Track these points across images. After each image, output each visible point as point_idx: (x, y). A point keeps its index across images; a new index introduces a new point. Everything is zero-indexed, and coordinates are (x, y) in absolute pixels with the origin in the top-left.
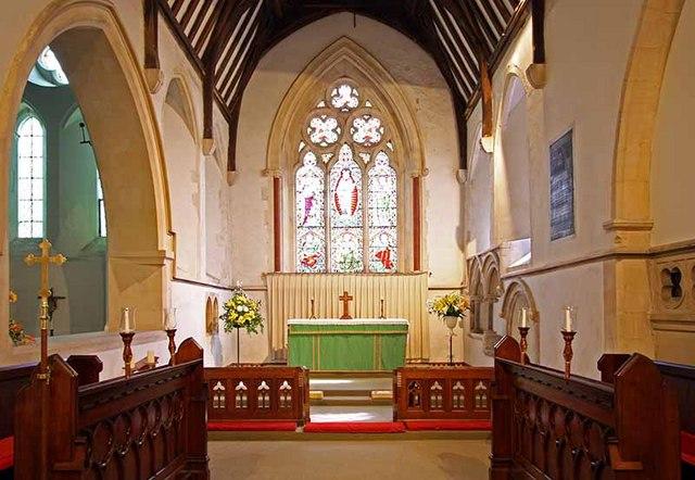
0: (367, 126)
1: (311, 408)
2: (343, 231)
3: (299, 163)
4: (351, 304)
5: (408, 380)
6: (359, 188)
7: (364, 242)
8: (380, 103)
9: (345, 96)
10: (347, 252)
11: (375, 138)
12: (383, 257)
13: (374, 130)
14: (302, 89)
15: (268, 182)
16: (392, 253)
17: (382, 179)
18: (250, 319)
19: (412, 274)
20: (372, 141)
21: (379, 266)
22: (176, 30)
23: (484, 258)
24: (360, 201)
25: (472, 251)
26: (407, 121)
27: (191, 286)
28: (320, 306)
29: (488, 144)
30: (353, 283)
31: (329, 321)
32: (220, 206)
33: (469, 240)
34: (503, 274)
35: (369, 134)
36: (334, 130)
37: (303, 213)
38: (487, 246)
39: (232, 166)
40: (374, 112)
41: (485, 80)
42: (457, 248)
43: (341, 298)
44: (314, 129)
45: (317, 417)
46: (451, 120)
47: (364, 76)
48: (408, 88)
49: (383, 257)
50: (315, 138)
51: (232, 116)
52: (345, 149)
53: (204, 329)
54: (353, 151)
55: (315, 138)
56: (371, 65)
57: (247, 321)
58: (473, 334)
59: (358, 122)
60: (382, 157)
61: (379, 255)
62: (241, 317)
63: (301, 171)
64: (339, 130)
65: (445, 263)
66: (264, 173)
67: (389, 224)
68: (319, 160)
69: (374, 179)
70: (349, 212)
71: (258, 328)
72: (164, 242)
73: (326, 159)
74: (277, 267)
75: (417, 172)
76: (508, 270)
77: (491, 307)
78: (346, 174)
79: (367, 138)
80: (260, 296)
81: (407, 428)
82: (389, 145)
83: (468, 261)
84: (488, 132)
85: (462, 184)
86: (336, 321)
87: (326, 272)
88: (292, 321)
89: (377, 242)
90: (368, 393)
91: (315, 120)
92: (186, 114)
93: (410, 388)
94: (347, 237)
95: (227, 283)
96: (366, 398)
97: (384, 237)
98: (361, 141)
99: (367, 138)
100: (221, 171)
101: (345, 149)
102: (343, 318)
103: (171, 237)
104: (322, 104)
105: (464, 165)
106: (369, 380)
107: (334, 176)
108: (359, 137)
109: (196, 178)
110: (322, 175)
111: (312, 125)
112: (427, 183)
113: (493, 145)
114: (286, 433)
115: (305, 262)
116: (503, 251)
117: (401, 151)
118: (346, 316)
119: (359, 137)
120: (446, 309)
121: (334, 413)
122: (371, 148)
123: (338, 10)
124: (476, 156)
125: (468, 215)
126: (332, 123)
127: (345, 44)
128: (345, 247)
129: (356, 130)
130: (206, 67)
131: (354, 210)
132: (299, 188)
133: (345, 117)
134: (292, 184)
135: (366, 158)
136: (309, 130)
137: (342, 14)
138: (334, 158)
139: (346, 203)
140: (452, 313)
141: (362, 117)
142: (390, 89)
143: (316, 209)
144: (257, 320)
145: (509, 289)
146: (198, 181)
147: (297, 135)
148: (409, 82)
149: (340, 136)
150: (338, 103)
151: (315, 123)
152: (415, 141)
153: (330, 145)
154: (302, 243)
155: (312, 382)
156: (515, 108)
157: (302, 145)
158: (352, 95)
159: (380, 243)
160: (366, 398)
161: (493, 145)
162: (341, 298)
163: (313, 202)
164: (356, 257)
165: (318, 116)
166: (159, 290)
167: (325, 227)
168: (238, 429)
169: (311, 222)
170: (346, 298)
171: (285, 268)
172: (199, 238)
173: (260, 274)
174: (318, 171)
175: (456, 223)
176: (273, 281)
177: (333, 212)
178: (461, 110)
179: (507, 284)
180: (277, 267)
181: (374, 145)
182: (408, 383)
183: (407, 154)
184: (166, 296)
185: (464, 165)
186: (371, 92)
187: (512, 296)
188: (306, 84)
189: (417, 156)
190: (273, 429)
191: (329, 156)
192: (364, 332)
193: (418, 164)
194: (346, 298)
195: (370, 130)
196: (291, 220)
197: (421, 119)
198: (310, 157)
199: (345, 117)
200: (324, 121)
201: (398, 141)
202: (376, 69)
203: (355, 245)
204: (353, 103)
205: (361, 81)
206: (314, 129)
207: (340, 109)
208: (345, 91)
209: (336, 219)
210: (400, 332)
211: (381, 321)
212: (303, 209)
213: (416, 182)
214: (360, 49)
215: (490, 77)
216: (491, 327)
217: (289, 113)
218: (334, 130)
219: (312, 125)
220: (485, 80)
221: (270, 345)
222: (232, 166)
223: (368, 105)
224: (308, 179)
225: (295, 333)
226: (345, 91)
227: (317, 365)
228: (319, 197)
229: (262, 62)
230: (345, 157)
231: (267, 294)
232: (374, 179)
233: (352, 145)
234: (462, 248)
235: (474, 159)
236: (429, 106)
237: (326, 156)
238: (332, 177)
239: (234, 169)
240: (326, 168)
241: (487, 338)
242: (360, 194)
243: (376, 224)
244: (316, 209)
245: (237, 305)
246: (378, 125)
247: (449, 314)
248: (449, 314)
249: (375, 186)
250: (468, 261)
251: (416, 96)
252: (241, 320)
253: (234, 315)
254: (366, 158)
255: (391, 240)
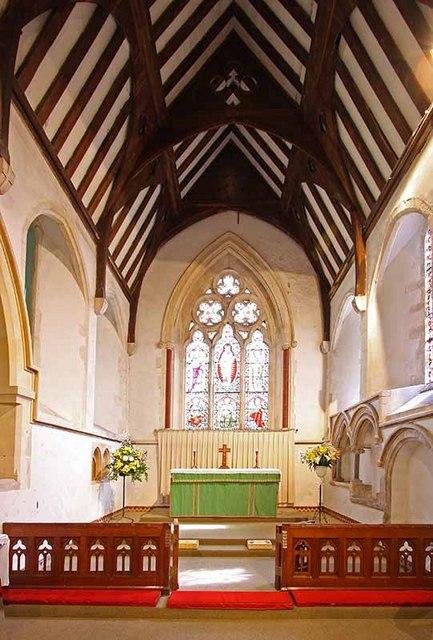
0: (246, 309)
1: (181, 561)
2: (224, 395)
3: (188, 338)
4: (229, 455)
5: (295, 540)
6: (238, 360)
7: (239, 404)
8: (257, 290)
9: (229, 285)
10: (226, 413)
11: (252, 319)
12: (257, 417)
13: (251, 312)
14: (193, 277)
15: (161, 354)
16: (264, 415)
17: (257, 353)
18: (134, 468)
19: (281, 431)
20: (250, 321)
21: (253, 425)
22: (117, 272)
23: (352, 413)
24: (238, 371)
25: (333, 409)
26: (279, 302)
27: (72, 434)
28: (201, 458)
29: (361, 301)
30: (231, 438)
31: (244, 471)
32: (119, 371)
33: (331, 401)
34: (383, 422)
35: (247, 316)
36: (219, 313)
37: (190, 381)
38: (354, 399)
39: (131, 338)
40: (253, 297)
41: (360, 243)
42: (319, 407)
43: (221, 450)
44: (202, 312)
45: (192, 578)
46: (316, 301)
47: (248, 269)
48: (282, 274)
49: (257, 417)
50: (203, 319)
51: (133, 296)
52: (228, 328)
53: (90, 477)
54: (234, 330)
55: (203, 319)
56: (251, 255)
57: (132, 470)
58: (337, 483)
59: (238, 306)
60: (257, 335)
61: (253, 415)
62: (126, 466)
63: (191, 346)
64: (223, 313)
65: (310, 421)
66: (159, 345)
67: (261, 390)
68: (206, 337)
69: (251, 353)
70: (230, 380)
71: (143, 476)
72: (20, 379)
73: (211, 336)
74: (167, 425)
75: (287, 344)
76: (388, 418)
77: (358, 457)
78: (228, 348)
79: (246, 319)
80: (151, 449)
81: (296, 604)
82: (263, 324)
83: (331, 418)
84: (360, 290)
85: (325, 354)
86: (216, 471)
87: (209, 429)
88: (173, 471)
89: (251, 405)
90: (244, 543)
91: (203, 304)
92: (75, 268)
93: (298, 549)
94: (227, 401)
95: (124, 436)
96: (241, 548)
97: (258, 401)
98: (240, 321)
99: (246, 319)
100: (118, 339)
101: (228, 328)
102: (222, 467)
103: (31, 376)
104: (209, 291)
105: (327, 336)
106: (244, 525)
107: (218, 350)
108: (239, 319)
109: (84, 331)
110: (208, 348)
111: (201, 309)
112: (295, 354)
113: (368, 303)
114: (145, 609)
115: (192, 421)
116: (384, 400)
117: (274, 329)
118: (224, 466)
119: (239, 319)
120: (318, 460)
121: (208, 567)
122: (249, 327)
123: (225, 209)
124: (339, 329)
125: (331, 380)
126: (217, 307)
127: (229, 239)
128: (225, 408)
129: (237, 312)
130: (102, 232)
131: (233, 378)
132: (188, 360)
133: (227, 302)
134: (183, 355)
135: (245, 335)
136: (198, 312)
137: (228, 212)
138: (218, 333)
139: (227, 372)
140: (324, 463)
141: (242, 301)
142: (267, 276)
143: (202, 378)
144: (142, 469)
145: (393, 437)
146: (86, 335)
147: (189, 318)
148: (282, 269)
149: (223, 318)
150: (222, 291)
151: (204, 307)
152: (286, 319)
153: (215, 324)
154: (190, 401)
155: (183, 527)
156: (395, 260)
157: (192, 325)
158: (235, 284)
159: (254, 407)
160: (241, 548)
161: (368, 303)
162: (221, 450)
163: (200, 372)
164: (234, 417)
165: (205, 301)
166: (10, 433)
167: (209, 392)
168: (85, 603)
169: (198, 388)
170: (224, 450)
171: (174, 425)
172: (85, 389)
173: (153, 431)
174: (206, 347)
175: (318, 387)
176: (164, 436)
177: (216, 380)
178: (326, 292)
179: (388, 433)
180: (167, 425)
181: (251, 324)
182: (294, 544)
183: (279, 330)
184: (21, 444)
185: (327, 336)
186: (250, 281)
187: (395, 443)
188: (197, 271)
189: (287, 331)
190: (129, 604)
191: (214, 333)
192: (239, 481)
193: (289, 339)
194: (224, 450)
195: (248, 312)
196: (181, 386)
197: (293, 303)
198: (198, 335)
199: (227, 302)
200: (210, 305)
201: (271, 321)
202: (255, 259)
203: (232, 407)
204: (235, 290)
205: (243, 272)
206: (202, 312)
207: (224, 295)
208: (229, 281)
209: (219, 386)
210: (272, 481)
211: (256, 471)
212: (191, 378)
213: (286, 353)
214: (243, 243)
215: (365, 238)
216: (357, 476)
217: (181, 295)
218: (219, 313)
219: (201, 309)
220: (360, 243)
221: (159, 491)
222: (131, 338)
223: (247, 291)
224: (197, 351)
225: (177, 481)
226: (229, 281)
227: (196, 510)
228: (205, 367)
229: (161, 253)
230: (228, 335)
231: (157, 448)
232: (251, 353)
233: (234, 325)
234: (324, 407)
235: (337, 332)
236: (297, 292)
237: (211, 333)
238: (216, 350)
239: (134, 342)
240: (211, 343)
241: (354, 487)
242: (238, 365)
243: (251, 390)
244: (202, 378)
245: (123, 454)
246: (255, 309)
247: (321, 464)
248: (321, 464)
249: (251, 358)
250: (331, 418)
251: (287, 281)
252: (127, 469)
253: (120, 464)
254: (245, 335)
255: (263, 403)
